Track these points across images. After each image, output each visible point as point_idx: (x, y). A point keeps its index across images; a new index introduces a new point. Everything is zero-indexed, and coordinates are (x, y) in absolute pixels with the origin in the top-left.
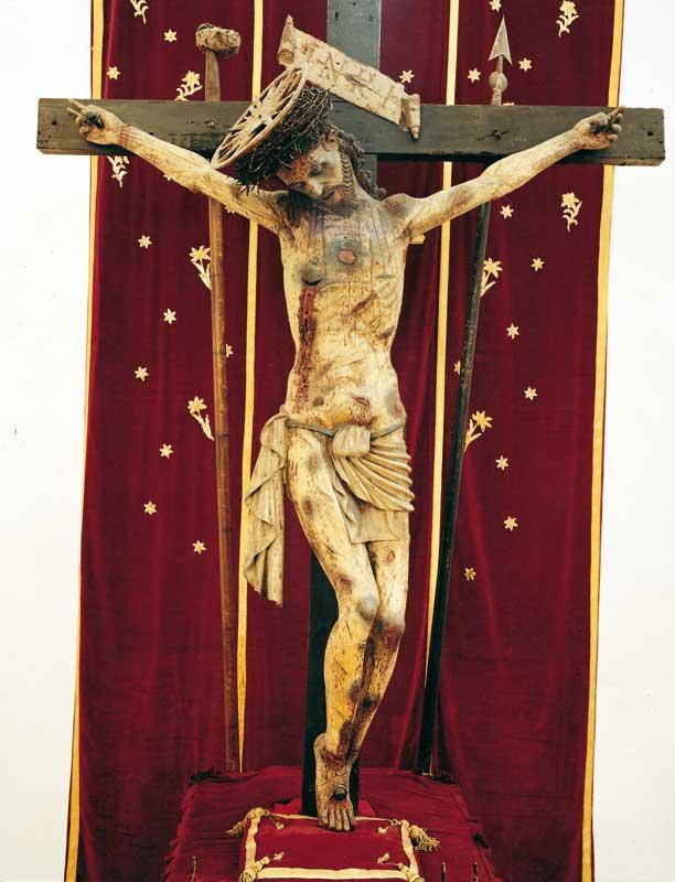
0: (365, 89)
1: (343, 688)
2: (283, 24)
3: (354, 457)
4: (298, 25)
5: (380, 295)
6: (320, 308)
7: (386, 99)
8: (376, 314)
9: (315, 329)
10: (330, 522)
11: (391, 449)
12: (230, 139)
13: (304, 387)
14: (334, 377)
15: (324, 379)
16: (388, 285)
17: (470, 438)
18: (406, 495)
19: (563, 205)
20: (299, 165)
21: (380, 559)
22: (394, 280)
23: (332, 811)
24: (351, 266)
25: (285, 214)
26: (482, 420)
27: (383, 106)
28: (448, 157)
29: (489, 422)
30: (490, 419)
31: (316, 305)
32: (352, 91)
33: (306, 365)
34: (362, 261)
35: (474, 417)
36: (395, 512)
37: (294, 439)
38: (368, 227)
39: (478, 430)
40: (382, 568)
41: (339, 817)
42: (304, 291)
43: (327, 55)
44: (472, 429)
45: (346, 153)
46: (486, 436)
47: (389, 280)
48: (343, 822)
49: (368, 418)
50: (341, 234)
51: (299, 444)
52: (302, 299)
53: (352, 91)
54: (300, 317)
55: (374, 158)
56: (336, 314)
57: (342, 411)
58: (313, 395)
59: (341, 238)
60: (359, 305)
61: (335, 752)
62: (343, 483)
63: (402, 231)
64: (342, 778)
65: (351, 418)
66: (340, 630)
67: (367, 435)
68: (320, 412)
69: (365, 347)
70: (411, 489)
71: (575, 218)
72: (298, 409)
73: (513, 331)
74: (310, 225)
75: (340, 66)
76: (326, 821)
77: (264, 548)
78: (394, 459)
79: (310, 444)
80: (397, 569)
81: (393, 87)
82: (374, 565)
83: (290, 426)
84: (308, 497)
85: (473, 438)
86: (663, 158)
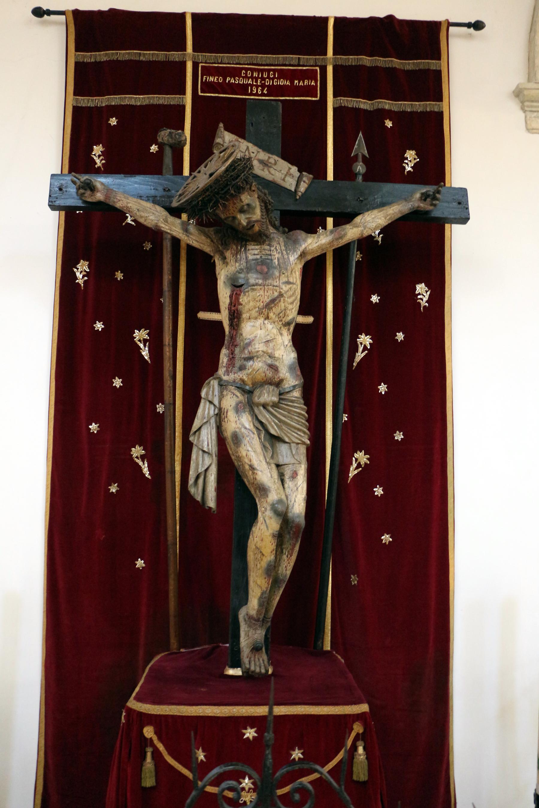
0: (272, 169)
1: (261, 567)
2: (216, 128)
3: (268, 405)
4: (227, 129)
5: (285, 295)
6: (244, 303)
7: (286, 175)
8: (283, 308)
9: (240, 318)
10: (252, 448)
11: (292, 401)
12: (185, 188)
13: (232, 359)
14: (253, 351)
15: (246, 352)
16: (291, 288)
17: (353, 472)
18: (304, 433)
19: (417, 292)
20: (232, 205)
21: (287, 477)
22: (294, 286)
23: (252, 659)
24: (266, 276)
25: (220, 242)
26: (361, 457)
27: (284, 180)
28: (330, 215)
29: (368, 459)
30: (368, 456)
31: (241, 300)
32: (263, 170)
33: (233, 344)
34: (273, 272)
35: (356, 455)
36: (298, 444)
37: (225, 393)
38: (277, 250)
39: (359, 465)
40: (289, 484)
41: (258, 664)
42: (233, 291)
43: (245, 148)
44: (355, 465)
45: (263, 201)
46: (365, 470)
47: (292, 285)
48: (260, 667)
49: (277, 380)
51: (229, 396)
52: (231, 297)
53: (263, 170)
54: (230, 309)
55: (279, 212)
56: (255, 308)
57: (259, 374)
58: (238, 364)
61: (255, 616)
62: (261, 423)
64: (259, 634)
65: (265, 379)
66: (259, 524)
67: (277, 391)
68: (243, 375)
69: (275, 331)
70: (307, 421)
71: (427, 302)
72: (227, 372)
73: (383, 388)
74: (237, 248)
76: (248, 666)
77: (203, 469)
78: (295, 407)
79: (237, 396)
80: (299, 484)
81: (290, 169)
82: (283, 481)
83: (223, 385)
84: (236, 432)
85: (356, 472)
86: (469, 219)
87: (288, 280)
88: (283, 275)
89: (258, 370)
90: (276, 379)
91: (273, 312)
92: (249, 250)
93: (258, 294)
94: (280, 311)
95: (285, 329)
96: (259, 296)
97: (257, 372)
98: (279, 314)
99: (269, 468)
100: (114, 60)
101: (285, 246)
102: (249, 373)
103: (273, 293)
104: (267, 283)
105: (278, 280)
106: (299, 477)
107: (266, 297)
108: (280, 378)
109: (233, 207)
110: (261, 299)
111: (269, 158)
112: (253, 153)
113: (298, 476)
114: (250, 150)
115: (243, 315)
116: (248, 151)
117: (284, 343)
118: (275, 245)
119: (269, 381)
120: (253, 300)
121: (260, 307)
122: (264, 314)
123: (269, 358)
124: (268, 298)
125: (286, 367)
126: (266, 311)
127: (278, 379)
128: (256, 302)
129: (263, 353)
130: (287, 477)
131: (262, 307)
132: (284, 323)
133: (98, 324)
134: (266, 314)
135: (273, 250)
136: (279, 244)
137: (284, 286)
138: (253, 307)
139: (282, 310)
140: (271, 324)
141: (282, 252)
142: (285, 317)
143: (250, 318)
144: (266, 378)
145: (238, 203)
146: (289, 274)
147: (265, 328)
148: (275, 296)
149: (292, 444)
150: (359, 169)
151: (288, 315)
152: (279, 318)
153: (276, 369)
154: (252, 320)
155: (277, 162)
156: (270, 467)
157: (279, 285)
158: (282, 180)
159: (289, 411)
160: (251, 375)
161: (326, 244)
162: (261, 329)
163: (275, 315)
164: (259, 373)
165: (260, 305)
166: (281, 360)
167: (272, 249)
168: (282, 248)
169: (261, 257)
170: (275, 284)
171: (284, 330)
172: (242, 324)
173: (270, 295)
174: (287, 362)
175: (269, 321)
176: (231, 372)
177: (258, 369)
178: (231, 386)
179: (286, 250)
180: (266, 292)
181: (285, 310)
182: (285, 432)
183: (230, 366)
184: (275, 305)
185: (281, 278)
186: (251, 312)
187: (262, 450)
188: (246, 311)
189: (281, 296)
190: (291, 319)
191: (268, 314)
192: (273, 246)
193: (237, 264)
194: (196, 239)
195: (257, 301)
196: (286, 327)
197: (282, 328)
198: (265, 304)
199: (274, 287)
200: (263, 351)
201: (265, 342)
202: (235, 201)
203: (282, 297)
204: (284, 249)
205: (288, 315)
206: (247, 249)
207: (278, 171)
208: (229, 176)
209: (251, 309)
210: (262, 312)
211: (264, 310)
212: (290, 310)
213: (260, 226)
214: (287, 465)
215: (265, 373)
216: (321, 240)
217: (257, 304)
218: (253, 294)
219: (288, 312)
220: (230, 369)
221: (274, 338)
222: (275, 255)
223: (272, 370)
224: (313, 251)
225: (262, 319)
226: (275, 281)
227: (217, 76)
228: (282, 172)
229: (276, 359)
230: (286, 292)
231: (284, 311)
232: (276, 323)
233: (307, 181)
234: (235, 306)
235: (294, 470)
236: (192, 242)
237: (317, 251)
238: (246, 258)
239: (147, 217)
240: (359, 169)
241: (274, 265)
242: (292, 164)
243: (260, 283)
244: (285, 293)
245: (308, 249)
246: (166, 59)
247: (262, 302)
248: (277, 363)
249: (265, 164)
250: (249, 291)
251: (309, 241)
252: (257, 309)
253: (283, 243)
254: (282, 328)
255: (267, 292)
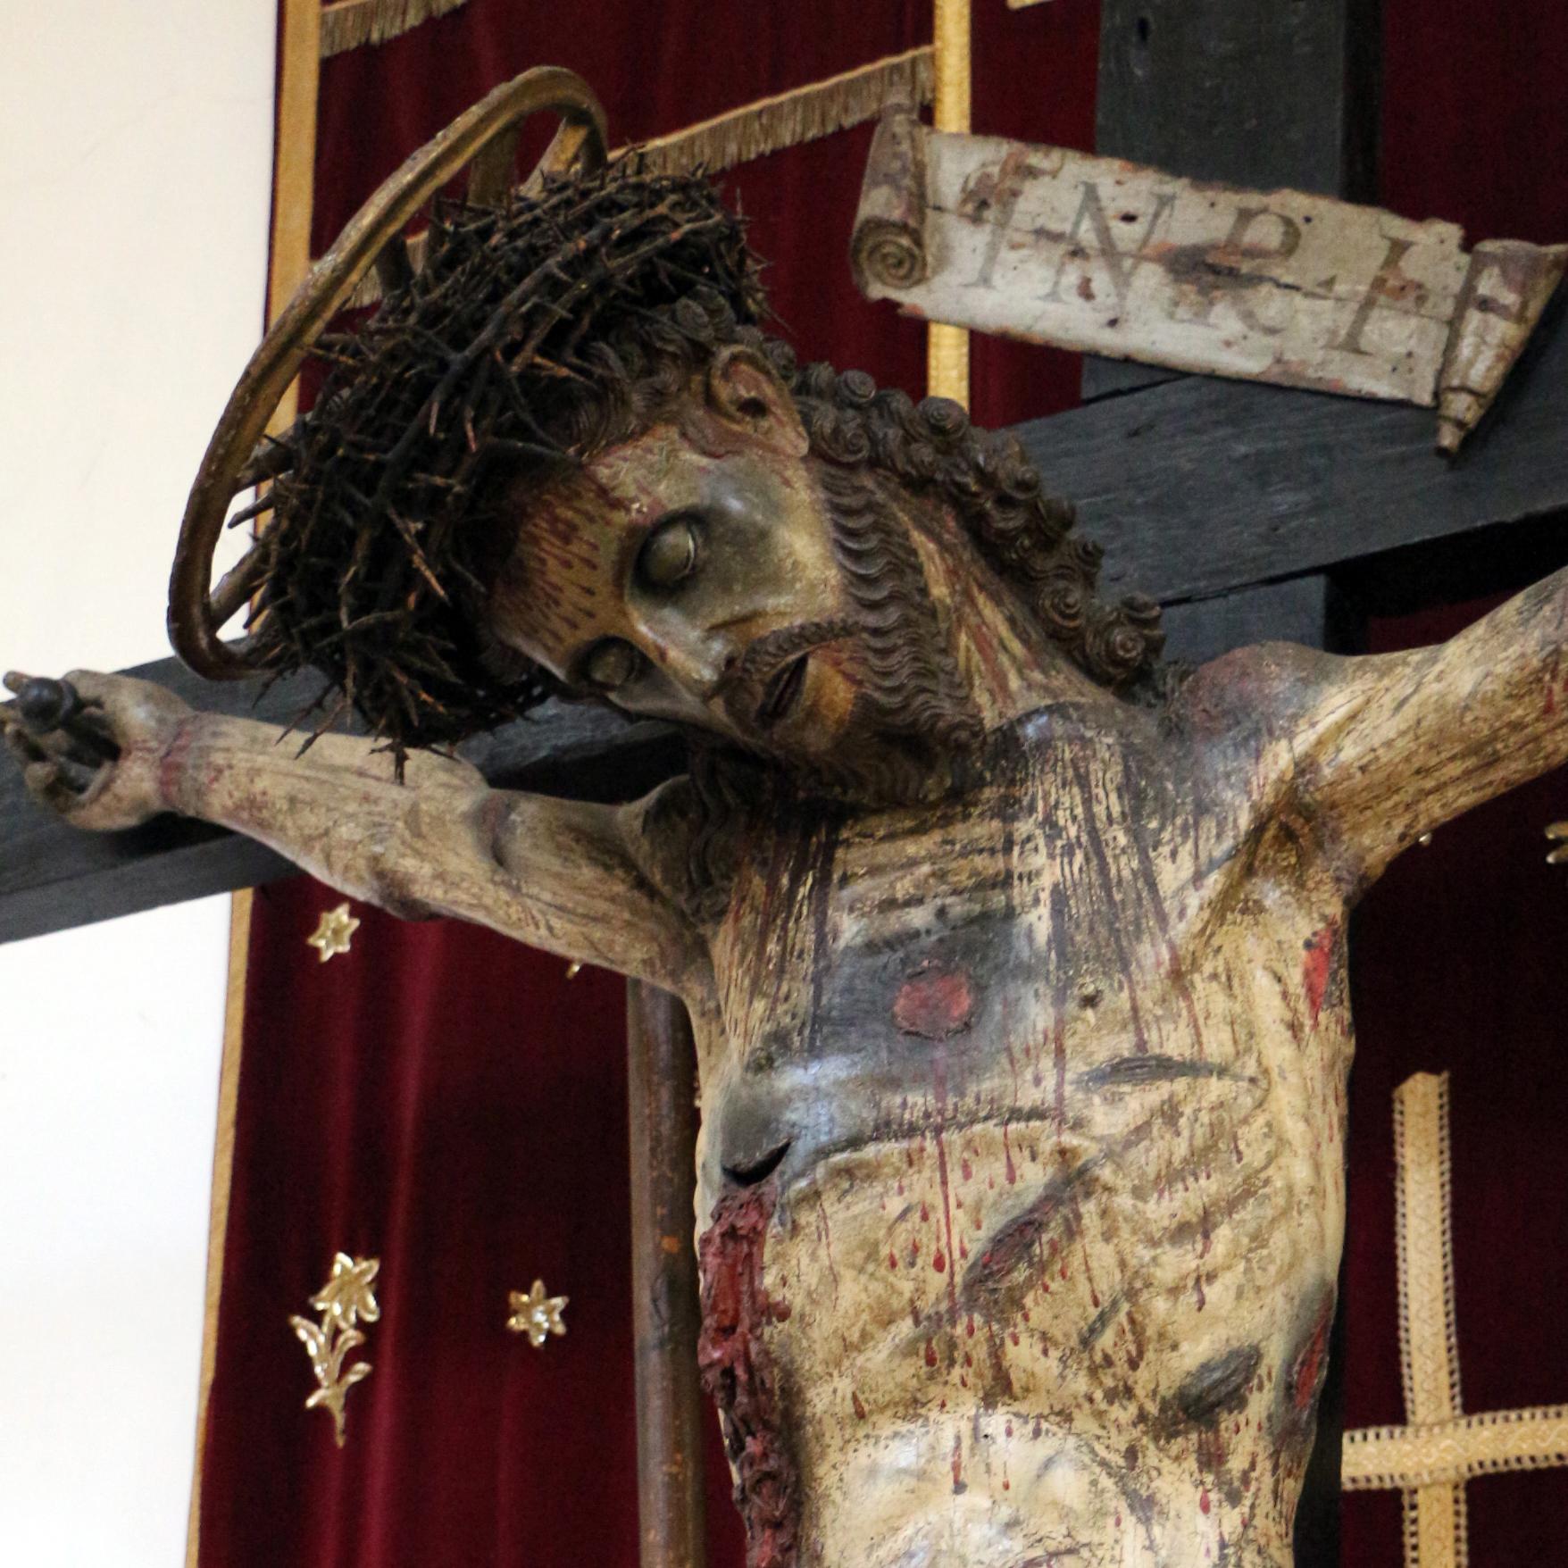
5: (1106, 1173)
6: (798, 1302)
8: (1109, 1281)
16: (1170, 1113)
27: (1352, 345)
43: (1077, 198)
47: (1181, 1085)
50: (915, 901)
56: (886, 1320)
60: (998, 1242)
63: (1245, 821)
69: (1068, 1484)
74: (773, 886)
75: (1137, 230)
81: (1399, 248)
87: (1142, 1045)
88: (1089, 1014)
91: (1031, 1332)
92: (845, 880)
93: (895, 1205)
94: (1093, 1313)
95: (1177, 1459)
96: (903, 1216)
98: (1086, 1342)
103: (1012, 1179)
104: (970, 1101)
105: (1047, 1063)
107: (960, 1217)
109: (567, 565)
110: (924, 1238)
111: (1245, 216)
112: (1129, 218)
114: (1105, 202)
115: (811, 1394)
116: (1093, 218)
118: (1046, 795)
120: (860, 1256)
121: (926, 1306)
122: (968, 1361)
124: (979, 1227)
126: (980, 1335)
128: (883, 1271)
131: (944, 1306)
132: (1153, 1409)
134: (981, 1353)
135: (1029, 839)
136: (1083, 781)
137: (1097, 1100)
138: (865, 1316)
139: (1105, 1302)
140: (1037, 1433)
141: (1094, 833)
142: (1150, 1355)
143: (861, 1415)
146: (1146, 1000)
148: (1030, 1199)
151: (1162, 1335)
152: (1093, 1371)
154: (886, 1426)
155: (1304, 228)
157: (1060, 1099)
158: (1341, 347)
161: (1488, 701)
162: (959, 1487)
163: (1054, 1354)
165: (920, 1291)
167: (1023, 827)
168: (1099, 810)
169: (941, 913)
170: (1029, 1097)
171: (1167, 1465)
172: (821, 1470)
173: (992, 1195)
175: (1017, 1407)
179: (1133, 818)
180: (955, 1176)
181: (1131, 1294)
184: (1043, 1267)
185: (1069, 1043)
186: (860, 1360)
188: (820, 1355)
189: (1078, 1188)
190: (1205, 1367)
191: (996, 1353)
192: (1032, 809)
193: (760, 1006)
194: (559, 901)
195: (893, 1264)
196: (1177, 1445)
197: (1151, 1456)
198: (958, 1279)
199: (1013, 1126)
202: (567, 514)
203: (1088, 1195)
204: (1116, 810)
205: (1162, 1335)
206: (836, 877)
207: (1309, 295)
208: (412, 319)
209: (854, 1336)
210: (952, 1345)
211: (960, 1330)
212: (1174, 1291)
213: (860, 672)
216: (1439, 678)
217: (893, 1289)
218: (856, 1210)
221: (1068, 1542)
225: (969, 1404)
228: (1341, 288)
230: (1115, 1152)
232: (1084, 1422)
233: (1510, 298)
234: (726, 1331)
237: (1421, 772)
239: (326, 833)
241: (1025, 954)
242: (1416, 211)
243: (918, 1113)
244: (1109, 1155)
245: (1327, 772)
247: (939, 1265)
249: (1214, 270)
250: (817, 1194)
252: (905, 1327)
253: (1116, 772)
254: (1151, 1456)
255: (967, 1175)
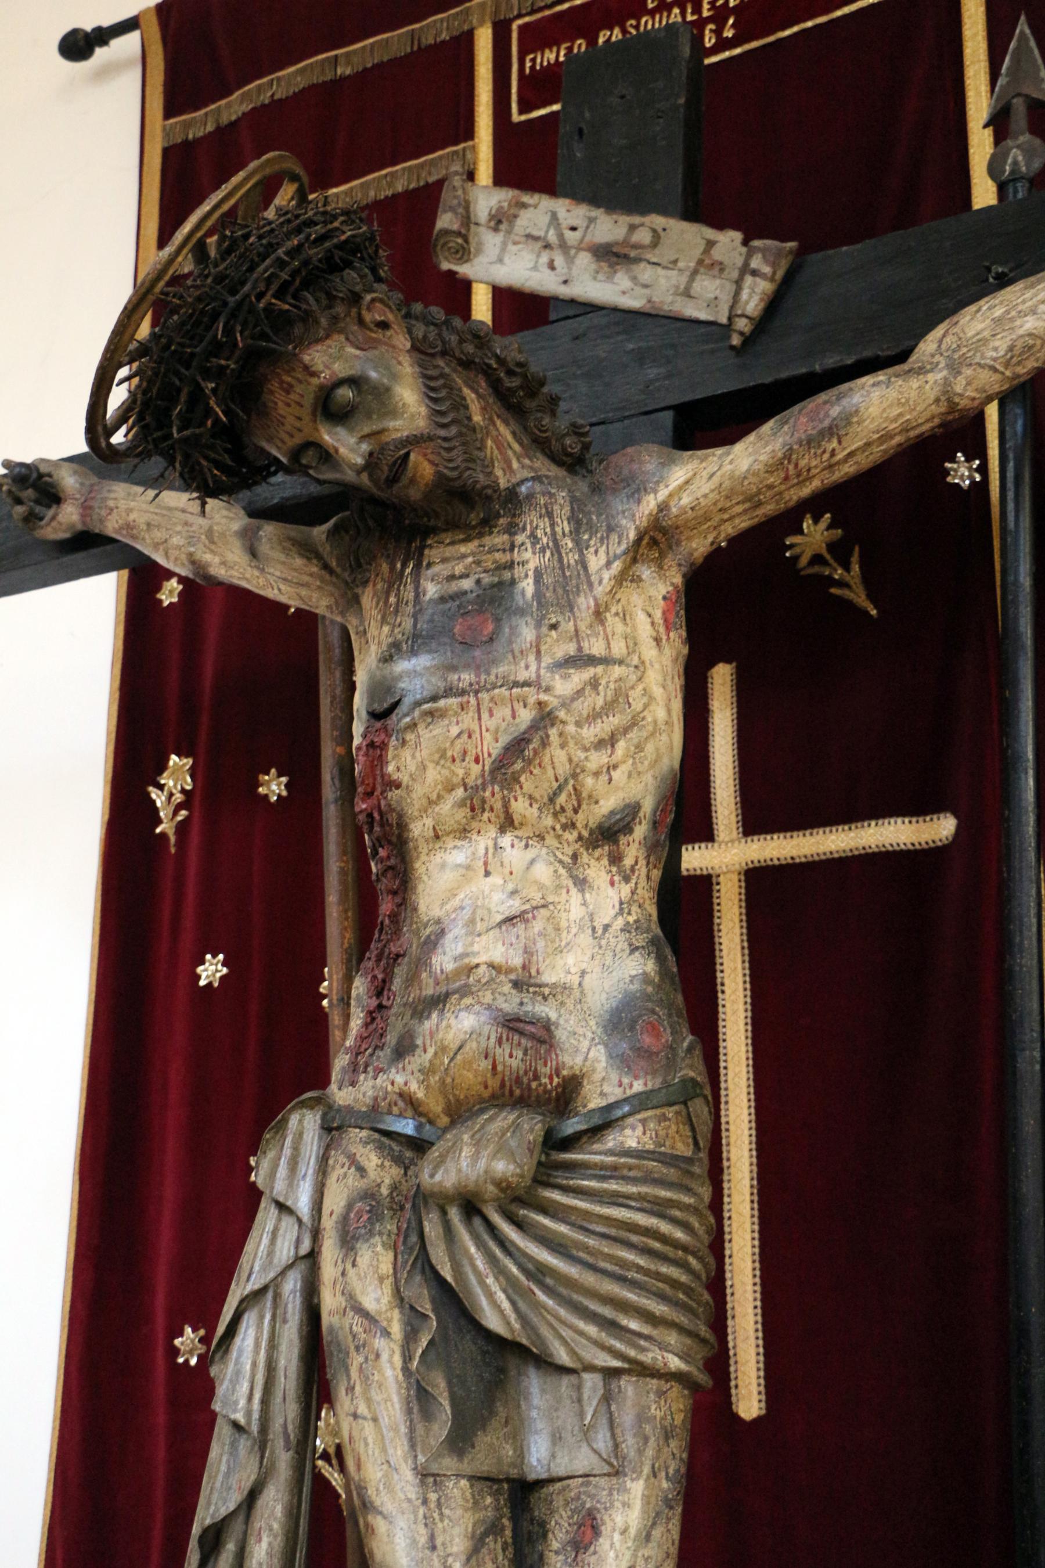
5: (562, 714)
6: (404, 778)
8: (563, 769)
27: (687, 294)
43: (547, 219)
47: (600, 669)
49: (548, 1082)
57: (467, 1064)
59: (467, 584)
60: (507, 749)
65: (494, 1083)
69: (543, 872)
74: (392, 568)
75: (577, 235)
78: (615, 1199)
81: (710, 244)
87: (580, 649)
88: (553, 633)
89: (460, 1048)
90: (545, 1080)
91: (524, 795)
93: (455, 730)
94: (555, 785)
96: (459, 736)
97: (456, 1054)
98: (552, 800)
99: (425, 1502)
100: (263, 106)
101: (573, 518)
102: (427, 1065)
103: (514, 717)
104: (493, 677)
105: (532, 658)
106: (603, 1543)
108: (565, 1073)
109: (288, 405)
111: (632, 228)
113: (601, 1540)
114: (561, 221)
115: (412, 826)
116: (555, 229)
117: (592, 921)
118: (531, 522)
119: (517, 1092)
120: (437, 756)
121: (471, 781)
122: (492, 809)
123: (514, 992)
124: (497, 741)
125: (592, 1023)
126: (498, 796)
127: (556, 1080)
128: (448, 764)
129: (494, 972)
130: (555, 1545)
131: (479, 782)
132: (585, 834)
133: (217, 971)
134: (498, 805)
135: (523, 544)
136: (550, 515)
137: (557, 677)
138: (439, 787)
139: (561, 779)
140: (527, 846)
141: (555, 541)
142: (584, 806)
143: (437, 837)
144: (499, 1077)
145: (300, 381)
147: (502, 865)
148: (523, 727)
149: (586, 1376)
150: (1015, 163)
151: (590, 797)
152: (555, 815)
153: (541, 1033)
154: (450, 843)
155: (662, 234)
156: (433, 1497)
157: (538, 676)
158: (681, 294)
159: (580, 1221)
160: (434, 1073)
161: (756, 474)
162: (487, 874)
163: (536, 806)
164: (464, 1062)
165: (467, 774)
166: (577, 993)
167: (520, 538)
168: (558, 530)
169: (478, 582)
170: (523, 675)
171: (593, 862)
173: (504, 725)
174: (604, 996)
176: (365, 1072)
177: (458, 1043)
178: (357, 1130)
179: (576, 534)
180: (485, 716)
181: (575, 776)
182: (549, 1317)
183: (364, 1046)
184: (530, 762)
185: (543, 648)
186: (437, 809)
187: (409, 1411)
188: (417, 807)
190: (612, 813)
191: (506, 805)
192: (524, 529)
193: (386, 629)
194: (284, 576)
195: (454, 760)
196: (597, 853)
197: (585, 858)
198: (487, 768)
199: (514, 690)
200: (491, 965)
201: (500, 925)
203: (553, 725)
204: (567, 530)
205: (590, 797)
206: (424, 564)
207: (665, 268)
209: (434, 797)
210: (484, 801)
211: (488, 794)
212: (596, 774)
214: (561, 1479)
215: (491, 1060)
216: (731, 463)
217: (453, 773)
219: (589, 781)
220: (362, 1060)
221: (542, 902)
222: (527, 562)
223: (523, 1041)
224: (701, 517)
225: (492, 832)
226: (522, 664)
227: (564, 41)
229: (547, 991)
231: (571, 782)
232: (550, 840)
233: (767, 270)
234: (369, 794)
235: (588, 1505)
236: (279, 590)
238: (417, 596)
240: (1015, 163)
242: (719, 225)
243: (466, 684)
244: (563, 705)
246: (412, 47)
248: (547, 1010)
250: (415, 725)
251: (678, 475)
252: (460, 792)
253: (567, 509)
254: (585, 858)
255: (491, 715)
